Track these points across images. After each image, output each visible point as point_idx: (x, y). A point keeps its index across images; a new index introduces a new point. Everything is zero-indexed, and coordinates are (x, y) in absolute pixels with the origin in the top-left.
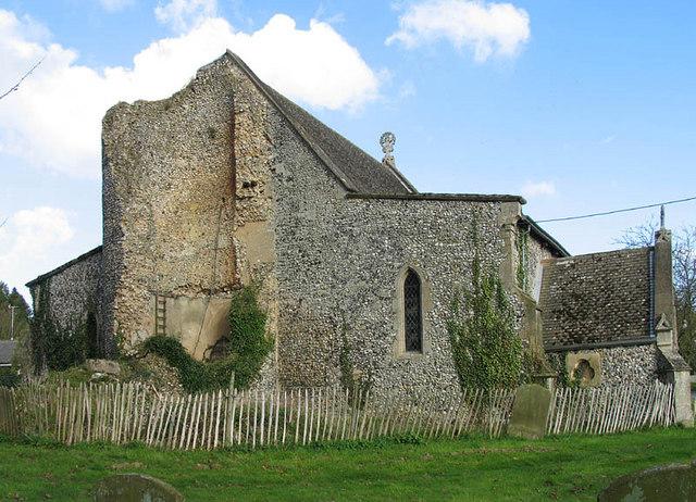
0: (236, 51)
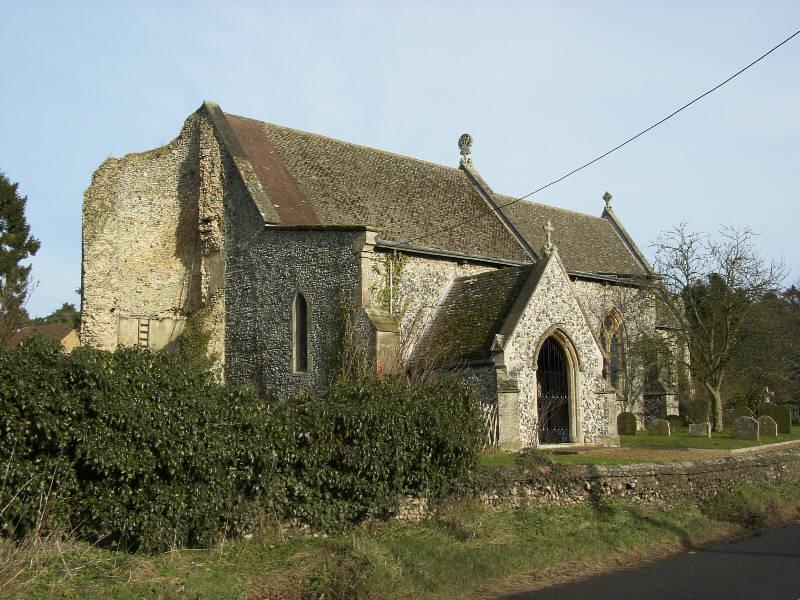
0: (213, 99)
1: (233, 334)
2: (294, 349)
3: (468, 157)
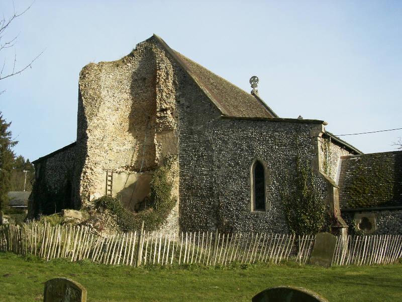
0: (160, 35)
1: (187, 184)
2: (252, 196)
3: (256, 89)
